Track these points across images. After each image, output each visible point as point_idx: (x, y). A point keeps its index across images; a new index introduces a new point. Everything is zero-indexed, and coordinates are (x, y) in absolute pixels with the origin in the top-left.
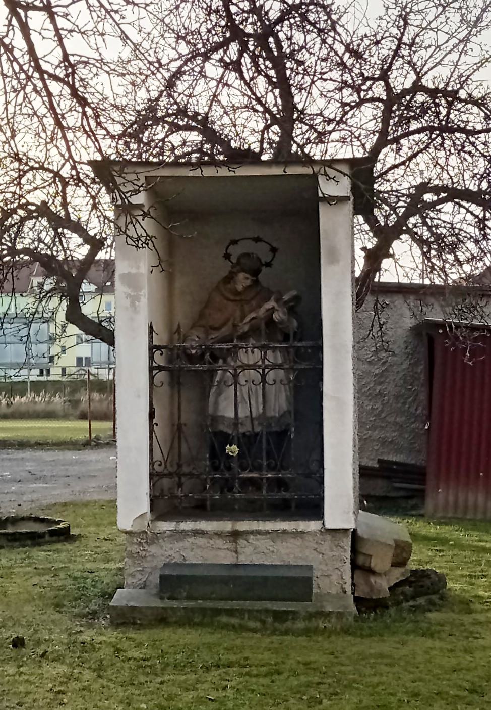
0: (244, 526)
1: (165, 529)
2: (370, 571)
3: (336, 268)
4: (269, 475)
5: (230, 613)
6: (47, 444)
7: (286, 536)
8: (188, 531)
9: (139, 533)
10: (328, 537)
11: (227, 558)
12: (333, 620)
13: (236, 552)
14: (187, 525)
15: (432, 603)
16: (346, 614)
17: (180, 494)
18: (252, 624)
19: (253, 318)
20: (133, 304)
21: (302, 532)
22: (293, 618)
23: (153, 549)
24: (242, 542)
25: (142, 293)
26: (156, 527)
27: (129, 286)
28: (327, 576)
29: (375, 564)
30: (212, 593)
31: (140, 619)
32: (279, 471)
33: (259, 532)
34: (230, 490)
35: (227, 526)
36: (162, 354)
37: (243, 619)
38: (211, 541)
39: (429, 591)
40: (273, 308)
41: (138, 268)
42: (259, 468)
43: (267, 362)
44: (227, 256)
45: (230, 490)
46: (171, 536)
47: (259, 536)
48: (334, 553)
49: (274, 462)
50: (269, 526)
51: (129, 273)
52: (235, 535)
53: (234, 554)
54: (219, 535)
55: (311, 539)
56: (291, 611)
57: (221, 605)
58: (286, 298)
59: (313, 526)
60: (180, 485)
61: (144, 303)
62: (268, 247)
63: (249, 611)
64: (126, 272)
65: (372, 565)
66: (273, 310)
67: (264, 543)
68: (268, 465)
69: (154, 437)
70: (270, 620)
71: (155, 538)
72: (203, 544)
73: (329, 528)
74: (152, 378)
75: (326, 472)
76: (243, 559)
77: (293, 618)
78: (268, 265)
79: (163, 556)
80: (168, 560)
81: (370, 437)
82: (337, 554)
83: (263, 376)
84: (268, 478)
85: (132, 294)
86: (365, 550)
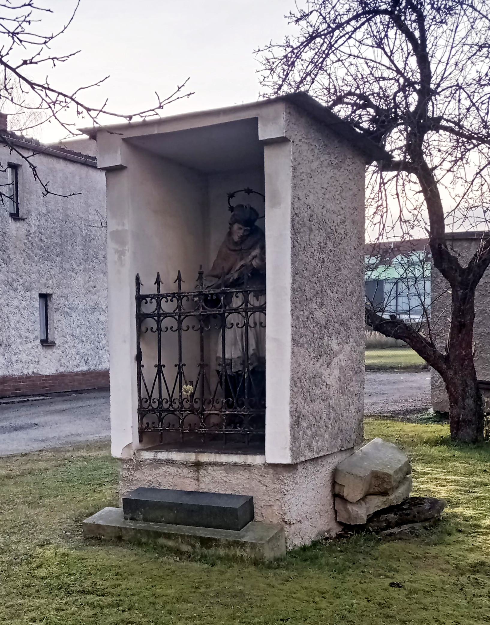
0: (204, 458)
1: (147, 457)
2: (344, 500)
4: (227, 412)
5: (168, 536)
6: (397, 368)
7: (237, 468)
8: (163, 460)
9: (128, 460)
10: (271, 471)
11: (190, 486)
12: (248, 550)
13: (198, 480)
14: (163, 455)
15: (413, 532)
16: (258, 544)
17: (160, 428)
18: (185, 548)
19: (242, 266)
20: (120, 258)
21: (250, 466)
22: (216, 545)
23: (138, 475)
24: (202, 472)
26: (140, 455)
28: (270, 506)
29: (347, 493)
30: (162, 517)
31: (104, 536)
33: (215, 464)
35: (192, 457)
36: (167, 302)
37: (177, 542)
38: (179, 470)
39: (416, 519)
41: (123, 225)
43: (249, 306)
46: (150, 464)
47: (215, 468)
48: (275, 486)
49: (231, 399)
50: (224, 458)
52: (198, 465)
53: (196, 482)
54: (184, 464)
56: (214, 539)
57: (166, 529)
59: (257, 460)
60: (161, 420)
61: (128, 257)
63: (182, 536)
64: (115, 230)
67: (219, 474)
70: (198, 545)
71: (139, 465)
72: (173, 473)
73: (269, 463)
75: (267, 411)
76: (203, 488)
77: (216, 545)
79: (144, 480)
80: (148, 484)
82: (278, 487)
85: (120, 249)
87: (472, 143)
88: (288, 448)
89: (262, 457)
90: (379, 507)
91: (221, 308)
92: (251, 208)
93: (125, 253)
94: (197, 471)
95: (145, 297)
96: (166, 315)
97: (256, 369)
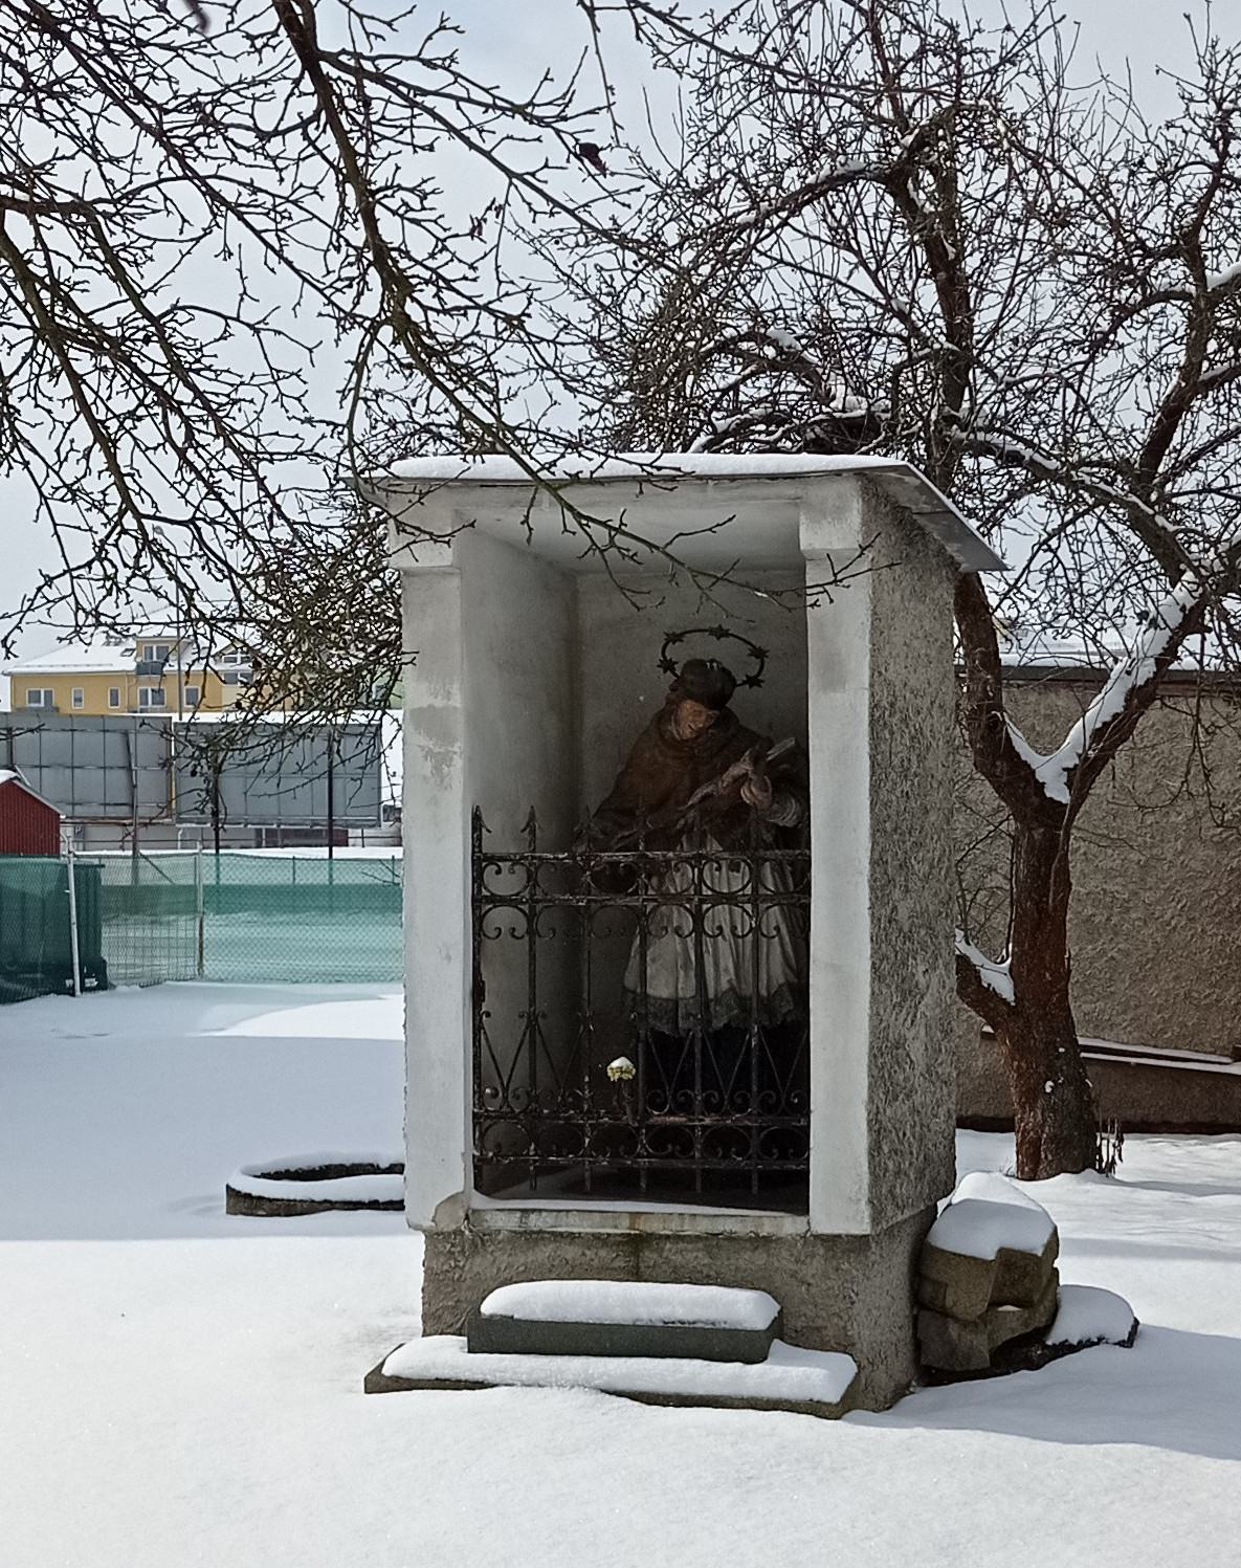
2: (945, 1314)
3: (839, 698)
20: (437, 769)
21: (767, 1240)
25: (456, 749)
27: (429, 734)
32: (728, 1114)
34: (631, 1152)
36: (499, 872)
38: (588, 1252)
40: (746, 775)
41: (448, 695)
42: (685, 1107)
44: (667, 665)
45: (631, 1152)
51: (431, 707)
55: (785, 1254)
58: (773, 754)
59: (787, 1225)
61: (458, 767)
62: (746, 649)
65: (949, 1302)
66: (741, 780)
68: (706, 1101)
69: (483, 1041)
74: (478, 920)
78: (753, 681)
81: (1217, 1001)
83: (699, 918)
84: (704, 1128)
85: (437, 750)
86: (936, 1271)
87: (146, 394)
88: (864, 1201)
89: (804, 1219)
90: (1013, 1330)
91: (635, 893)
92: (724, 670)
93: (451, 759)
94: (636, 1253)
95: (492, 859)
96: (497, 901)
97: (733, 1025)
